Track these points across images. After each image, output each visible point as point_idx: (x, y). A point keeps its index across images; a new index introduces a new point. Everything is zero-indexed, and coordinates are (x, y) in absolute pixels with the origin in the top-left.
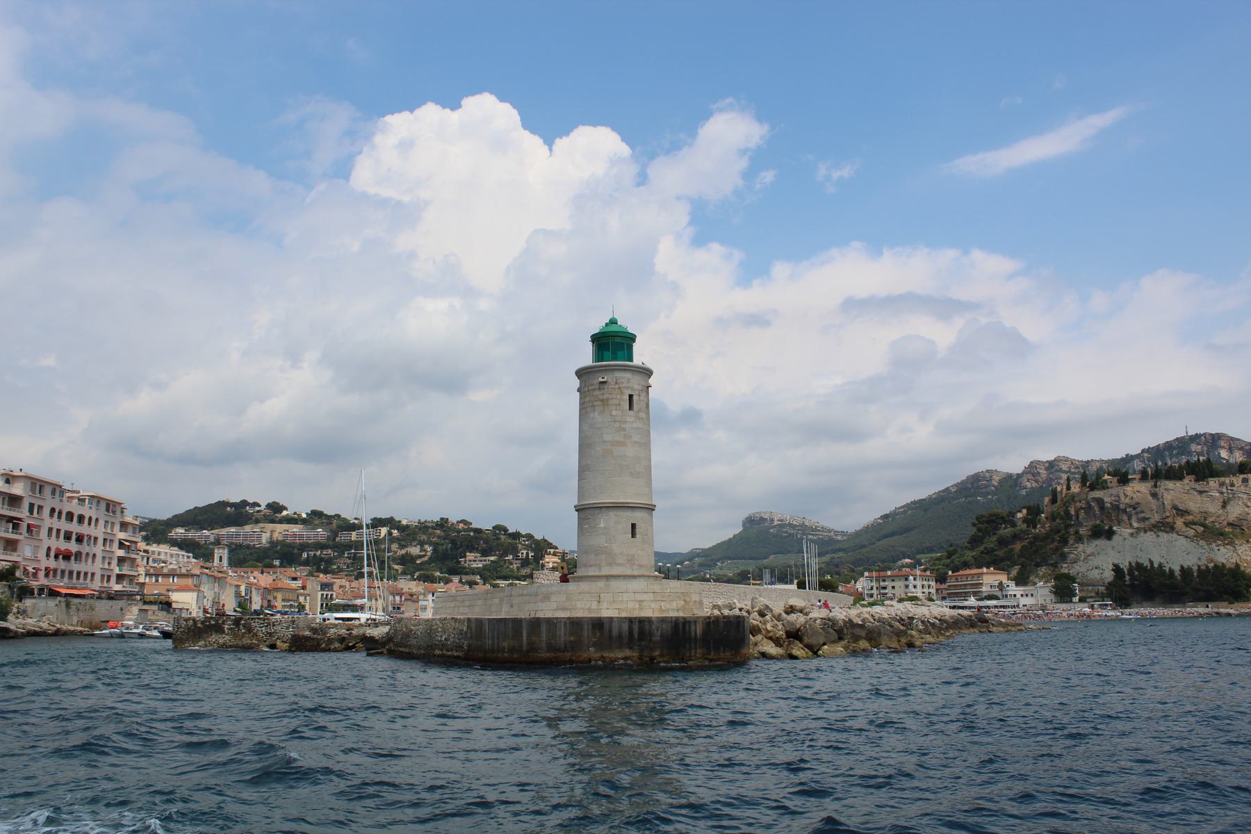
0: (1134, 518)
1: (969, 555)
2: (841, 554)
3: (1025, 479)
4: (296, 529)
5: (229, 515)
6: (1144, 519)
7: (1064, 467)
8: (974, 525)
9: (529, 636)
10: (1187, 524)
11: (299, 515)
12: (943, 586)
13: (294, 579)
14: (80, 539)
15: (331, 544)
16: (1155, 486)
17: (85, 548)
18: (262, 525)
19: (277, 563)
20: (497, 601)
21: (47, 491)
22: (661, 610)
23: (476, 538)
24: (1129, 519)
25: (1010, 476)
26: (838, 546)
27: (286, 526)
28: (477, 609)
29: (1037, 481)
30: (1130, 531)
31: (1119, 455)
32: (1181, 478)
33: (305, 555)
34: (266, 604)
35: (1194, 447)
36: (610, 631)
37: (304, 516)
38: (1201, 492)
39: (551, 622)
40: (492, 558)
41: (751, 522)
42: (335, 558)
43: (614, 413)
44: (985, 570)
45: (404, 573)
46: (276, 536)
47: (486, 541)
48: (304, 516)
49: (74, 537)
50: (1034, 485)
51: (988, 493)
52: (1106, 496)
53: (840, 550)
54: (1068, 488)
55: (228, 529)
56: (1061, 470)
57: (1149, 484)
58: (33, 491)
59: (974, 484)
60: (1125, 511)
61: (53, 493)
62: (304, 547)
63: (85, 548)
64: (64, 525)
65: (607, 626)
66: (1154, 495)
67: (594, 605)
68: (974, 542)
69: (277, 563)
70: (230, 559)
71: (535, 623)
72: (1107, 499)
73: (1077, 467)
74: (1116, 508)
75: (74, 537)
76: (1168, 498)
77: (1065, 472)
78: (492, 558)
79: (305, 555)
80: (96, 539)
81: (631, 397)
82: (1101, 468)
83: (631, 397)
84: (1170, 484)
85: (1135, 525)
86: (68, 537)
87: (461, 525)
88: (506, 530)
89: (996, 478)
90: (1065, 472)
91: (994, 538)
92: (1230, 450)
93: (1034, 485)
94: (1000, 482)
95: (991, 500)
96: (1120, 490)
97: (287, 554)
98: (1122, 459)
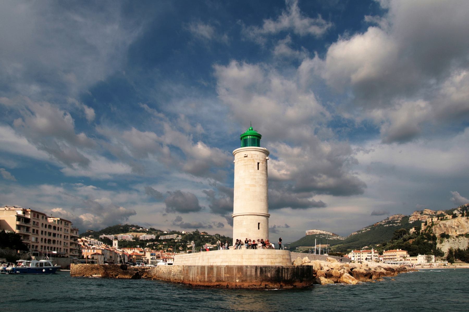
0: (458, 231)
2: (342, 245)
8: (394, 234)
9: (208, 274)
14: (54, 235)
17: (56, 239)
19: (139, 246)
20: (198, 258)
21: (40, 216)
22: (272, 263)
26: (341, 242)
28: (190, 262)
33: (148, 244)
36: (246, 273)
37: (147, 230)
39: (218, 268)
41: (363, 33)
45: (183, 250)
49: (52, 234)
51: (397, 223)
53: (342, 243)
58: (34, 216)
61: (43, 217)
63: (56, 239)
64: (48, 230)
65: (244, 269)
67: (240, 260)
69: (139, 246)
70: (118, 245)
71: (211, 268)
75: (52, 234)
79: (148, 244)
80: (61, 235)
86: (50, 234)
88: (220, 235)
91: (402, 239)
95: (399, 226)
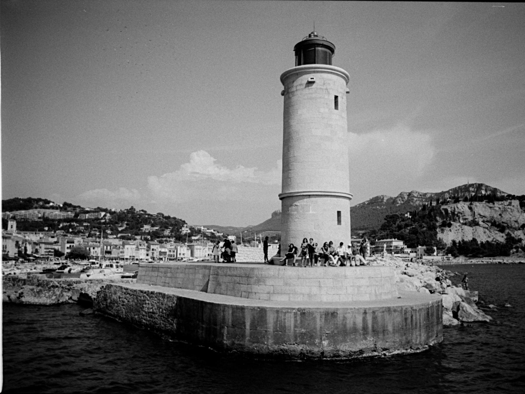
0: (461, 218)
1: (384, 233)
3: (398, 199)
4: (57, 212)
5: (21, 204)
6: (466, 219)
7: (416, 195)
10: (483, 222)
11: (59, 206)
12: (373, 246)
13: (53, 237)
15: (75, 219)
16: (471, 204)
18: (39, 210)
19: (46, 229)
23: (149, 218)
24: (459, 219)
25: (391, 198)
27: (51, 210)
29: (403, 201)
30: (459, 224)
31: (439, 191)
32: (482, 201)
33: (61, 225)
34: (34, 251)
35: (471, 189)
38: (491, 207)
40: (157, 228)
42: (77, 226)
43: (322, 110)
44: (393, 240)
46: (46, 215)
47: (154, 220)
48: (61, 206)
50: (402, 202)
52: (449, 208)
54: (431, 203)
55: (19, 212)
56: (414, 196)
57: (468, 203)
59: (376, 201)
60: (457, 216)
62: (60, 221)
66: (470, 208)
68: (384, 228)
69: (46, 229)
70: (17, 227)
72: (449, 210)
73: (421, 195)
74: (453, 213)
76: (476, 210)
77: (416, 197)
78: (157, 228)
79: (61, 225)
81: (336, 97)
82: (431, 197)
83: (336, 97)
84: (477, 203)
85: (462, 221)
87: (142, 212)
88: (163, 215)
89: (385, 199)
90: (416, 197)
92: (486, 191)
93: (402, 202)
94: (387, 200)
96: (453, 205)
97: (51, 225)
98: (440, 193)
